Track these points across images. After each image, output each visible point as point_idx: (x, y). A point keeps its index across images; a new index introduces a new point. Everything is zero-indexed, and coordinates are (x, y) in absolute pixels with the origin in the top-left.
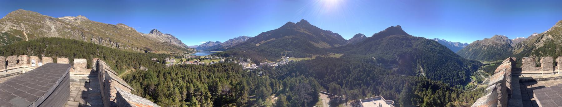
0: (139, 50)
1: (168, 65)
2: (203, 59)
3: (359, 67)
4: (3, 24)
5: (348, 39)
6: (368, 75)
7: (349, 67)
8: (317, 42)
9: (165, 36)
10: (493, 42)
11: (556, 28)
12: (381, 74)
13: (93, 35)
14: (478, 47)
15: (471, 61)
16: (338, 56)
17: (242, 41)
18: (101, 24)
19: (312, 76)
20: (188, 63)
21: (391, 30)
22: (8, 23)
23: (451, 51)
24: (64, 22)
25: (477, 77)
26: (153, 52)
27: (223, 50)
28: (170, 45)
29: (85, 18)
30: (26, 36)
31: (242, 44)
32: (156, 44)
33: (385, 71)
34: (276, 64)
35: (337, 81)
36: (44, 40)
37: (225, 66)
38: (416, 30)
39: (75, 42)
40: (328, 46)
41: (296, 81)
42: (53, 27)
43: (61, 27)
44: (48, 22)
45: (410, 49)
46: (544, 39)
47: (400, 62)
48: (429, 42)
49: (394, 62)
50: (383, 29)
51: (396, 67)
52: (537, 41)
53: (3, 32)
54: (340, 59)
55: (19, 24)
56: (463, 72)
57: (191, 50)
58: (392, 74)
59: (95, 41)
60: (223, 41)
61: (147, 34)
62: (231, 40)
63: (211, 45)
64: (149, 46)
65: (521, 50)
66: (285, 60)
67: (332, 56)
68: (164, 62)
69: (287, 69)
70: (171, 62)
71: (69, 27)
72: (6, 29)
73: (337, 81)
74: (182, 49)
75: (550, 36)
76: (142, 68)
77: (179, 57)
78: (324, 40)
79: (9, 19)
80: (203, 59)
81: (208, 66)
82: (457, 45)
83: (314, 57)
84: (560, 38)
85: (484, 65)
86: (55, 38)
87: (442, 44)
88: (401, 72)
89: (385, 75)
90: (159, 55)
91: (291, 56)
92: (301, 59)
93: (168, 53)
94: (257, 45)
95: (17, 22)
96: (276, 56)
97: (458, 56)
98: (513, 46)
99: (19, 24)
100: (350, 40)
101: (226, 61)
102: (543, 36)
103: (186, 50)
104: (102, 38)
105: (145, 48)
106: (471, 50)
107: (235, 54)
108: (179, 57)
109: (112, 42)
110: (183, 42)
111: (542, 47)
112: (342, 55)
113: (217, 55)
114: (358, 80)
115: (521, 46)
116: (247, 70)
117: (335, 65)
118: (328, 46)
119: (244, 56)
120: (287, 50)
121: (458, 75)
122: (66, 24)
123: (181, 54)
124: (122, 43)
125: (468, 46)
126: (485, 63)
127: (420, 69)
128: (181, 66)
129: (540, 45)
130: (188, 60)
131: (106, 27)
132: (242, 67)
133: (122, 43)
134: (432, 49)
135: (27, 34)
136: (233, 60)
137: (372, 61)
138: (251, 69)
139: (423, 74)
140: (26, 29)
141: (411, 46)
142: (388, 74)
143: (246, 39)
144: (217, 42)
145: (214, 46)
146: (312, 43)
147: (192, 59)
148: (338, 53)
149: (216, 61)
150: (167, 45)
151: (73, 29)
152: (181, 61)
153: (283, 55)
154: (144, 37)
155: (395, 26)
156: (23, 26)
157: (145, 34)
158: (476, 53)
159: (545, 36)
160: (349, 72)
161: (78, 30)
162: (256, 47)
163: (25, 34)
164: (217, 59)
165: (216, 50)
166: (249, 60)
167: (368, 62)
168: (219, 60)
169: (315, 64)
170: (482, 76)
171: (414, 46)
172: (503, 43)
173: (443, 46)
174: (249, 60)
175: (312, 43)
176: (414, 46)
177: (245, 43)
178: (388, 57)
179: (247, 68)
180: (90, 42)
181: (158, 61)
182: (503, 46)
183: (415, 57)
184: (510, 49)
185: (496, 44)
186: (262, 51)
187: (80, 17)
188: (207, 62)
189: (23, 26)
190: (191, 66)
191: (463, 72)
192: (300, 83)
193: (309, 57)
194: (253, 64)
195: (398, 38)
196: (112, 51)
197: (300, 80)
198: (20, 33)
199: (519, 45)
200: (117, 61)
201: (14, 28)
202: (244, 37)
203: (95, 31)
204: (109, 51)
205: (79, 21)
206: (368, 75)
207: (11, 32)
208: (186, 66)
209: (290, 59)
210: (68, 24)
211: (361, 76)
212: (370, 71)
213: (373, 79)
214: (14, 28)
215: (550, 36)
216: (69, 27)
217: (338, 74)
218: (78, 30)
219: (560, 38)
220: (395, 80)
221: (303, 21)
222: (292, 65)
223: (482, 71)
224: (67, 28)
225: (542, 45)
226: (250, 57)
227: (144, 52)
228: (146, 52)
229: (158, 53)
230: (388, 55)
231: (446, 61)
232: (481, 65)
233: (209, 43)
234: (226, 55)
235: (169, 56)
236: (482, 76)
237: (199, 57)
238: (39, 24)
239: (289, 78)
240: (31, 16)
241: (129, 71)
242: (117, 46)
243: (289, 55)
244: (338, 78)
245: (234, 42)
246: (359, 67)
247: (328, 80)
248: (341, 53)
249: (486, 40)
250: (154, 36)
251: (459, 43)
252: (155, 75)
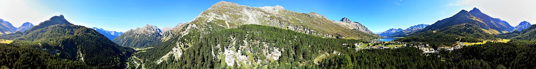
0: (330, 36)
1: (357, 49)
2: (388, 44)
3: (524, 51)
4: (208, 15)
5: (514, 26)
6: (34, 59)
7: (18, 52)
8: (488, 29)
9: (354, 23)
10: (144, 31)
11: (200, 18)
12: (45, 58)
13: (289, 24)
14: (132, 36)
15: (125, 48)
16: (505, 41)
17: (421, 28)
18: (296, 13)
19: (482, 59)
20: (374, 47)
21: (55, 19)
22: (212, 13)
23: (107, 39)
24: (264, 12)
25: (130, 63)
26: (343, 38)
27: (404, 36)
28: (359, 32)
29: (282, 8)
30: (228, 25)
31: (420, 31)
32: (346, 31)
33: (49, 55)
34: (452, 49)
35: (8, 65)
36: (244, 27)
37: (407, 50)
38: (75, 19)
39: (275, 28)
40: (497, 32)
41: (470, 63)
42: (250, 16)
43: (262, 16)
44: (246, 12)
45: (71, 37)
46: (189, 28)
47: (62, 48)
48: (88, 30)
49: (57, 47)
50: (48, 18)
51: (59, 52)
52: (183, 30)
53: (208, 22)
54: (508, 44)
55: (222, 15)
56: (118, 58)
57: (376, 36)
58: (55, 58)
59: (291, 28)
60: (404, 28)
61: (338, 22)
62: (412, 28)
63: (394, 31)
64: (340, 32)
65: (169, 38)
66: (460, 45)
67: (500, 41)
68: (354, 47)
69: (461, 52)
70: (359, 47)
71: (269, 16)
72: (211, 19)
73: (8, 65)
74: (368, 35)
75: (194, 26)
76: (335, 52)
77: (367, 43)
78: (493, 27)
79: (213, 10)
80: (388, 44)
81: (392, 50)
82: (113, 34)
83: (485, 42)
84: (203, 27)
85: (137, 52)
86: (255, 25)
87: (100, 32)
88: (63, 56)
89: (49, 59)
90: (349, 40)
91: (465, 41)
92: (473, 44)
93: (357, 38)
94: (434, 32)
95: (219, 12)
96: (452, 42)
97: (114, 43)
98: (161, 34)
99: (222, 15)
100: (19, 28)
101: (408, 45)
102: (188, 25)
103: (372, 36)
104: (297, 26)
105: (337, 34)
106: (125, 38)
107: (415, 40)
108: (367, 43)
109: (306, 30)
110: (369, 29)
111: (187, 35)
112: (12, 41)
113: (400, 40)
114: (522, 63)
115: (169, 34)
116: (427, 54)
117: (503, 49)
118: (497, 32)
119: (423, 41)
120: (461, 35)
121: (113, 61)
122: (266, 13)
123: (368, 40)
124: (315, 30)
125: (123, 35)
126: (137, 49)
127: (79, 54)
128: (369, 50)
129: (185, 33)
130: (374, 45)
131: (299, 16)
132: (422, 51)
133: (315, 30)
134: (91, 37)
135: (229, 23)
136: (414, 45)
137: (38, 46)
138: (429, 54)
139: (82, 59)
140: (228, 19)
141: (73, 34)
142: (52, 58)
143: (424, 27)
144: (399, 29)
145: (397, 33)
146: (483, 30)
147: (377, 44)
148: (506, 38)
149: (399, 46)
150: (355, 31)
151: (272, 18)
152: (368, 45)
153: (458, 40)
154: (336, 24)
155: (58, 15)
156: (224, 16)
157: (336, 22)
158: (129, 41)
159: (190, 25)
160: (515, 55)
161: (277, 18)
162: (433, 33)
163: (227, 23)
164: (399, 44)
165: (399, 36)
166: (427, 45)
167: (34, 47)
168: (401, 45)
169: (485, 48)
170: (135, 62)
171: (75, 34)
172: (153, 32)
173: (100, 35)
174: (427, 45)
175: (483, 30)
176: (75, 34)
177: (424, 30)
178: (52, 43)
179: (426, 52)
180: (287, 29)
181: (348, 46)
182: (153, 34)
183: (76, 43)
184: (159, 37)
185: (147, 33)
186: (438, 37)
187: (278, 7)
188: (391, 47)
189: (224, 16)
190: (378, 50)
191: (118, 58)
192: (473, 65)
193: (480, 42)
194: (431, 49)
195: (61, 27)
196: (307, 36)
197: (473, 62)
198: (223, 22)
199: (167, 34)
200: (312, 46)
201: (217, 18)
202: (422, 25)
203: (291, 20)
204: (305, 37)
205: (277, 11)
206: (34, 59)
207: (215, 21)
208: (373, 50)
209: (464, 44)
210: (268, 14)
211: (28, 59)
212: (36, 56)
213: (39, 62)
214: (217, 18)
215: (194, 26)
216: (269, 16)
217: (8, 58)
218: (277, 18)
219: (203, 27)
220: (58, 64)
221: (475, 9)
222: (466, 49)
223: (135, 57)
224: (266, 17)
225: (187, 33)
226: (429, 43)
227: (335, 38)
228: (337, 37)
229: (348, 38)
230: (52, 42)
231: (103, 47)
232: (134, 51)
233: (392, 30)
234: (407, 41)
235: (358, 42)
236: (135, 62)
237: (384, 42)
238: (239, 14)
239: (463, 61)
240: (231, 7)
241: (324, 55)
242: (311, 33)
243: (463, 41)
244: (506, 61)
245: (414, 29)
246: (27, 51)
247: (497, 62)
248: (509, 39)
249: (138, 29)
250: (344, 24)
251: (115, 32)
252: (349, 59)
